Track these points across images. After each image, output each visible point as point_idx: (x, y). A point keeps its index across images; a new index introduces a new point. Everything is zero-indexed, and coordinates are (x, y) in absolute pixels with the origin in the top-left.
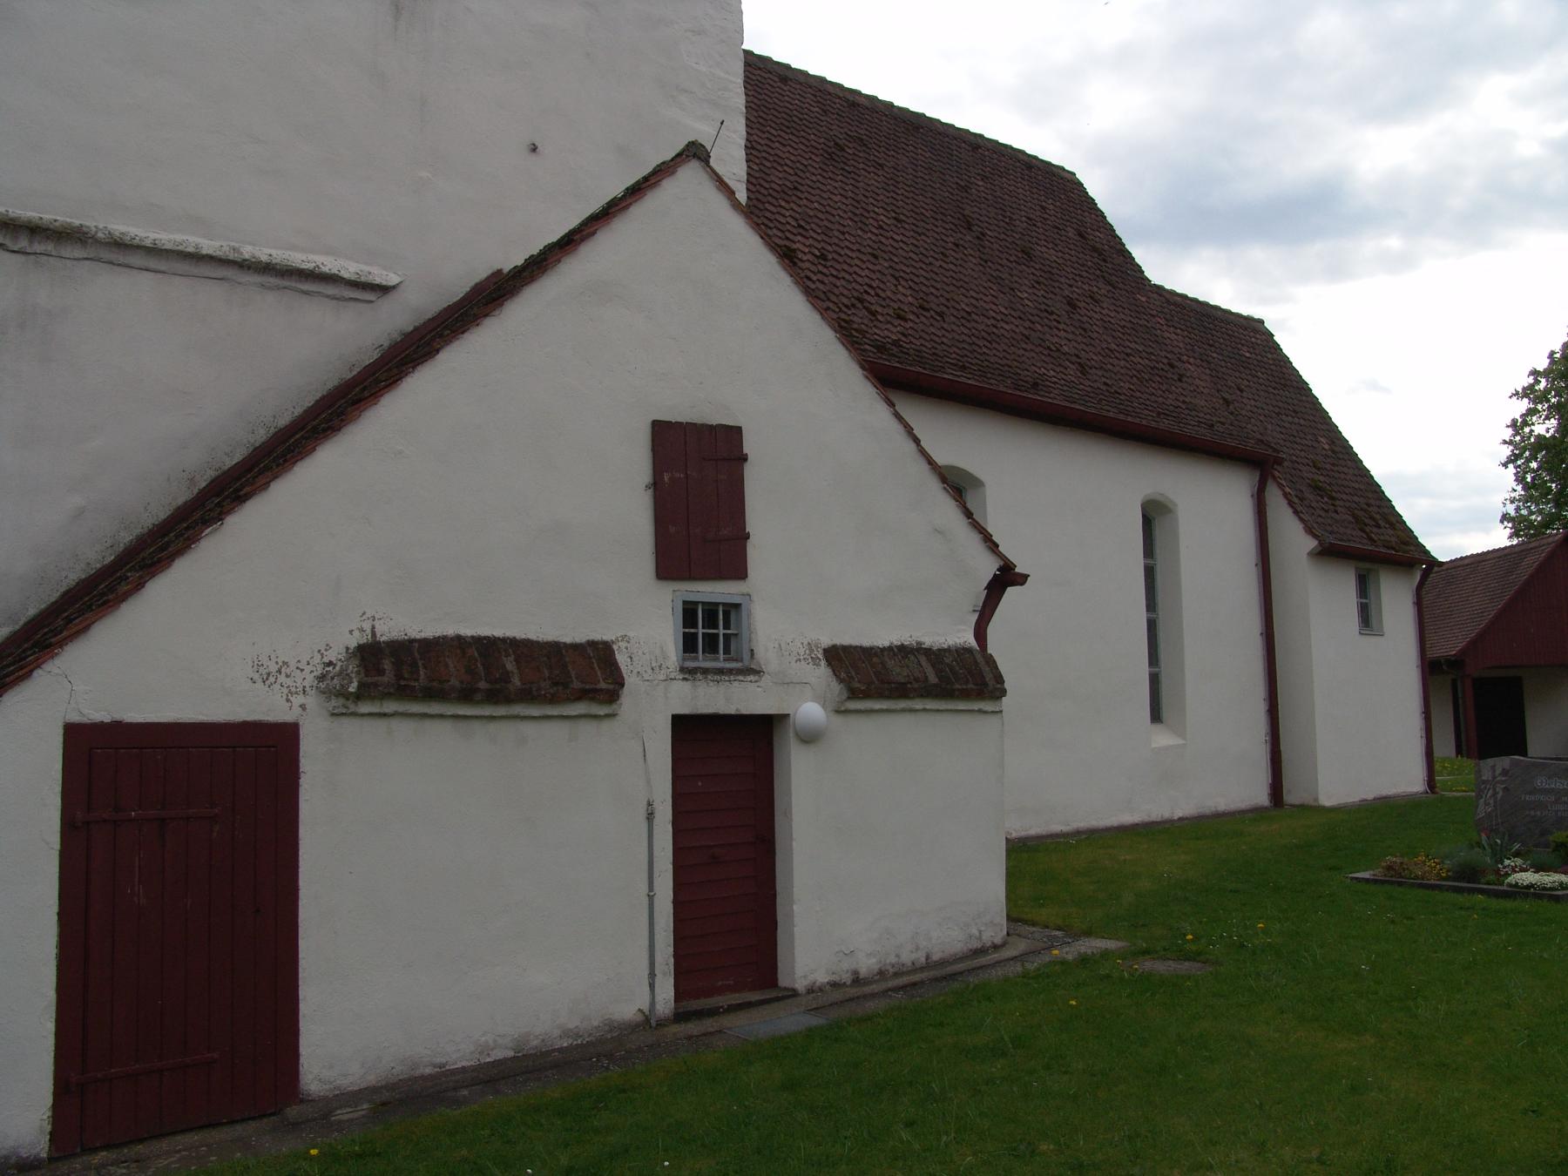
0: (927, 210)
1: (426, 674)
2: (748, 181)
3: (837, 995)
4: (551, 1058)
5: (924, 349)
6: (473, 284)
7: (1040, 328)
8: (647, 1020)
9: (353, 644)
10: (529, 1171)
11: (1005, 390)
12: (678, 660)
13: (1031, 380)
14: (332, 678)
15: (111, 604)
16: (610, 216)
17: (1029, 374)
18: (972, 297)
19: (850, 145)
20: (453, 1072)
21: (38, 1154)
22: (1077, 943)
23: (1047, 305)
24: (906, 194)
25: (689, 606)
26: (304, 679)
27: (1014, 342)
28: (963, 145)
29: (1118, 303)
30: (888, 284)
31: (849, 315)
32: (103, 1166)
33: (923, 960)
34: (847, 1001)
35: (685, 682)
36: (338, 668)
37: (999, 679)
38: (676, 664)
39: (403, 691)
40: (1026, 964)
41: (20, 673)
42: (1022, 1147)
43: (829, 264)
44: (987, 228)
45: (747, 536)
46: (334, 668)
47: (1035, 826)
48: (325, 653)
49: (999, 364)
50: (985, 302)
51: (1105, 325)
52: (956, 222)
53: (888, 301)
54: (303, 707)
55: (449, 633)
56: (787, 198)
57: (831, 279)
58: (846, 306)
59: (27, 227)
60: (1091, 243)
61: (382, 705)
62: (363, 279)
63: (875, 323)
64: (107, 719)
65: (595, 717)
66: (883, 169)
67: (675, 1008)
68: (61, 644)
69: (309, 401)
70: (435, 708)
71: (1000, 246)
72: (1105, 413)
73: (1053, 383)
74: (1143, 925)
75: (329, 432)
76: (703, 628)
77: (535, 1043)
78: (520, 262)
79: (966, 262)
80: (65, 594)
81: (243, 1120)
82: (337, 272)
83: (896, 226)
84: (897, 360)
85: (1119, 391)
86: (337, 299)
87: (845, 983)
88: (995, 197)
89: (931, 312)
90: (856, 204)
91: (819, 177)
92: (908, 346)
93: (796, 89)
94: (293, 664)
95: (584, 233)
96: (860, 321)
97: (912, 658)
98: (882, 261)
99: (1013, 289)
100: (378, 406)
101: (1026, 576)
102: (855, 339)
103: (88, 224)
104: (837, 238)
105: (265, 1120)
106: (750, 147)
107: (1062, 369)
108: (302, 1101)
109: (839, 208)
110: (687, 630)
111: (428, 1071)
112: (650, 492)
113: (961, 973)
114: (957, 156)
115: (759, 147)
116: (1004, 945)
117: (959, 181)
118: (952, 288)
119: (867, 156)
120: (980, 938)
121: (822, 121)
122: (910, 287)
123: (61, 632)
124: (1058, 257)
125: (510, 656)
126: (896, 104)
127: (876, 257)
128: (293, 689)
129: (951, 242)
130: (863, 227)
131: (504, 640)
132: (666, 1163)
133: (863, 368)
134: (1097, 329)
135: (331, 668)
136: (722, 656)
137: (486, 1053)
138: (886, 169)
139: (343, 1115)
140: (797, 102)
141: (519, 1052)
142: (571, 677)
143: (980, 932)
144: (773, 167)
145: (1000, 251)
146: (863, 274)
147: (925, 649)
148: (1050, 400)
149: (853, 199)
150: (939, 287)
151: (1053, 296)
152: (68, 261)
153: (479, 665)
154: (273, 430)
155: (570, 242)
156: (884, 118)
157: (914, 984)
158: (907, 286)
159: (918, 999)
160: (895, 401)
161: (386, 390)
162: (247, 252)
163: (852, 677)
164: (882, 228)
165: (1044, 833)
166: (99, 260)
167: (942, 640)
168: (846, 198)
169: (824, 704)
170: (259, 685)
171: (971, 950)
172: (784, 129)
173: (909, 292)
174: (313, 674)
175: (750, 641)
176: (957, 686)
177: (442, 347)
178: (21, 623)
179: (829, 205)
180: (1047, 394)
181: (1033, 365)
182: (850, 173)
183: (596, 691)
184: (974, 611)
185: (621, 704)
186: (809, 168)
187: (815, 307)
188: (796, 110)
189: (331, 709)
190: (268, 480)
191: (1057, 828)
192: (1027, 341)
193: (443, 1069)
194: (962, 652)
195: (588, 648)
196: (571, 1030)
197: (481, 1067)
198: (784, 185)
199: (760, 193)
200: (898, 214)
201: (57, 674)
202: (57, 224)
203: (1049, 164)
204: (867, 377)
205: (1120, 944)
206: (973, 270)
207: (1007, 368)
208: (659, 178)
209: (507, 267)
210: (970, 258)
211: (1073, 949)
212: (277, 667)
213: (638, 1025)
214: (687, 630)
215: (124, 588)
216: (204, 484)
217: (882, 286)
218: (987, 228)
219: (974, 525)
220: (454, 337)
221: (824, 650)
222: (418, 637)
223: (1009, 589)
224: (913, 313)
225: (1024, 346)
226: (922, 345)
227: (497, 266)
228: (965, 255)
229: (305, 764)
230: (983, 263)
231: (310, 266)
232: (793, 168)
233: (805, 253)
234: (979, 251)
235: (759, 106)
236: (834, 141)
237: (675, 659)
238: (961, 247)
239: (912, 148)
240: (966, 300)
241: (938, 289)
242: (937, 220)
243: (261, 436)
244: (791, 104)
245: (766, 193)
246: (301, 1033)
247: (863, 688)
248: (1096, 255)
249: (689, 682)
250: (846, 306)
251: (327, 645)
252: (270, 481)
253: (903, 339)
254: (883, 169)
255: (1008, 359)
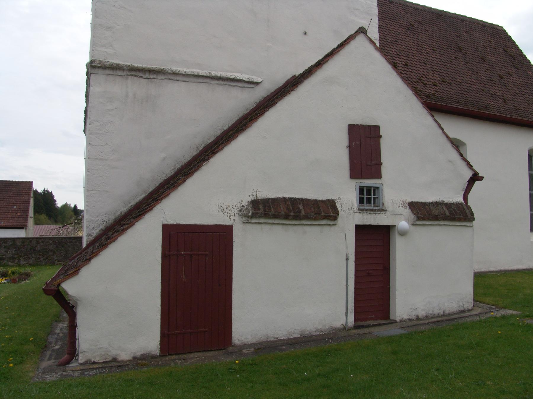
0: (444, 46)
1: (273, 210)
2: (379, 40)
3: (411, 323)
4: (312, 338)
5: (444, 96)
6: (286, 80)
7: (488, 87)
8: (345, 327)
9: (250, 200)
10: (306, 374)
11: (474, 110)
12: (357, 206)
13: (485, 106)
14: (243, 211)
15: (176, 187)
16: (333, 55)
17: (483, 103)
18: (462, 76)
19: (416, 24)
20: (280, 340)
21: (157, 354)
22: (501, 311)
23: (490, 78)
24: (437, 40)
25: (362, 188)
26: (235, 211)
27: (478, 92)
28: (458, 20)
29: (520, 75)
30: (430, 73)
31: (416, 85)
32: (175, 360)
33: (442, 313)
34: (414, 325)
35: (360, 214)
36: (245, 208)
37: (472, 214)
38: (357, 207)
39: (266, 215)
40: (481, 317)
41: (150, 208)
42: (480, 382)
43: (408, 67)
44: (467, 51)
45: (382, 164)
46: (244, 208)
47: (484, 268)
48: (241, 203)
49: (472, 101)
50: (467, 78)
51: (514, 84)
52: (456, 49)
53: (430, 79)
54: (234, 220)
55: (281, 197)
56: (393, 45)
57: (409, 73)
58: (415, 82)
59: (148, 70)
60: (509, 53)
61: (259, 220)
62: (250, 80)
63: (426, 87)
64: (175, 223)
65: (329, 225)
66: (428, 32)
67: (354, 324)
68: (161, 199)
69: (234, 121)
70: (276, 221)
71: (473, 57)
72: (514, 117)
73: (493, 106)
74: (527, 306)
75: (242, 131)
76: (366, 195)
77: (307, 333)
78: (302, 72)
79: (459, 63)
80: (160, 184)
81: (215, 350)
82: (242, 79)
83: (433, 52)
84: (434, 100)
85: (520, 108)
86: (242, 87)
87: (413, 319)
88: (471, 39)
89: (446, 82)
90: (418, 45)
91: (404, 36)
92: (438, 95)
93: (395, 5)
94: (231, 206)
95: (324, 61)
96: (420, 87)
97: (440, 206)
98: (428, 65)
99: (477, 73)
100: (257, 122)
101: (483, 177)
102: (418, 94)
103: (165, 68)
104: (411, 58)
105: (221, 351)
106: (380, 28)
107: (496, 101)
108: (233, 346)
109: (412, 47)
110: (360, 196)
111: (272, 339)
112: (348, 149)
113: (456, 319)
114: (456, 25)
115: (382, 27)
116: (472, 310)
117: (457, 34)
118: (454, 74)
119: (422, 27)
120: (463, 307)
121: (405, 16)
122: (438, 74)
123: (161, 196)
124: (495, 60)
125: (301, 204)
126: (432, 8)
127: (426, 64)
128: (231, 214)
129: (454, 57)
130: (421, 53)
131: (299, 199)
132: (352, 375)
133: (423, 104)
134: (511, 86)
135: (243, 208)
136: (372, 205)
137: (291, 335)
138: (429, 32)
139: (246, 351)
140: (396, 10)
141: (301, 336)
142: (321, 211)
143: (463, 304)
144: (388, 34)
145: (472, 59)
146: (421, 70)
147: (445, 203)
148: (492, 113)
149: (417, 43)
150: (449, 73)
151: (494, 75)
152: (160, 80)
153: (291, 207)
154: (222, 131)
155: (319, 64)
156: (428, 13)
157: (439, 321)
158: (437, 74)
159: (440, 327)
160: (434, 114)
161: (260, 116)
162: (214, 73)
163: (418, 212)
164: (428, 53)
165: (487, 271)
166: (169, 79)
167: (451, 200)
168: (415, 43)
169: (408, 222)
170: (221, 213)
171: (460, 311)
172: (391, 20)
173: (438, 76)
174: (237, 210)
175: (382, 200)
176: (456, 217)
177: (278, 102)
178: (148, 193)
179: (408, 46)
180: (490, 111)
181: (485, 100)
182: (416, 34)
183: (329, 216)
184: (463, 190)
185: (338, 221)
186: (401, 33)
187: (405, 83)
188: (396, 13)
189: (243, 221)
190: (223, 147)
191: (492, 269)
192: (482, 91)
193: (277, 339)
194: (458, 204)
195: (327, 202)
196: (319, 329)
197: (289, 339)
198: (392, 40)
199: (383, 43)
200: (434, 48)
201: (160, 209)
202: (157, 69)
203: (492, 24)
204: (424, 107)
205: (519, 313)
206: (462, 67)
207: (475, 102)
208: (349, 41)
209: (297, 74)
210: (461, 62)
211: (499, 313)
212: (226, 207)
213: (341, 329)
214: (360, 196)
215: (179, 182)
216: (201, 149)
217: (428, 74)
218: (467, 51)
219: (464, 159)
220: (282, 98)
221: (408, 203)
222: (271, 198)
223: (476, 182)
224: (439, 83)
225: (482, 93)
226: (443, 95)
227: (294, 74)
228: (459, 61)
229: (235, 239)
230: (466, 64)
231: (233, 77)
232: (395, 34)
233: (400, 64)
234: (464, 59)
235: (382, 13)
236: (410, 23)
237: (356, 206)
238: (457, 59)
239: (439, 23)
240: (459, 78)
241: (449, 74)
242: (448, 49)
243: (219, 133)
244: (394, 11)
245: (385, 43)
246: (233, 324)
247: (422, 217)
248: (511, 57)
249: (361, 214)
250: (415, 82)
251: (242, 200)
252: (224, 147)
253: (436, 93)
254: (428, 32)
255: (475, 99)
